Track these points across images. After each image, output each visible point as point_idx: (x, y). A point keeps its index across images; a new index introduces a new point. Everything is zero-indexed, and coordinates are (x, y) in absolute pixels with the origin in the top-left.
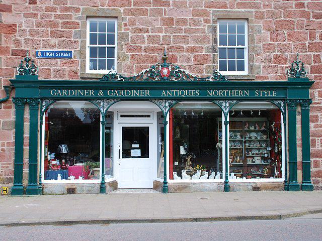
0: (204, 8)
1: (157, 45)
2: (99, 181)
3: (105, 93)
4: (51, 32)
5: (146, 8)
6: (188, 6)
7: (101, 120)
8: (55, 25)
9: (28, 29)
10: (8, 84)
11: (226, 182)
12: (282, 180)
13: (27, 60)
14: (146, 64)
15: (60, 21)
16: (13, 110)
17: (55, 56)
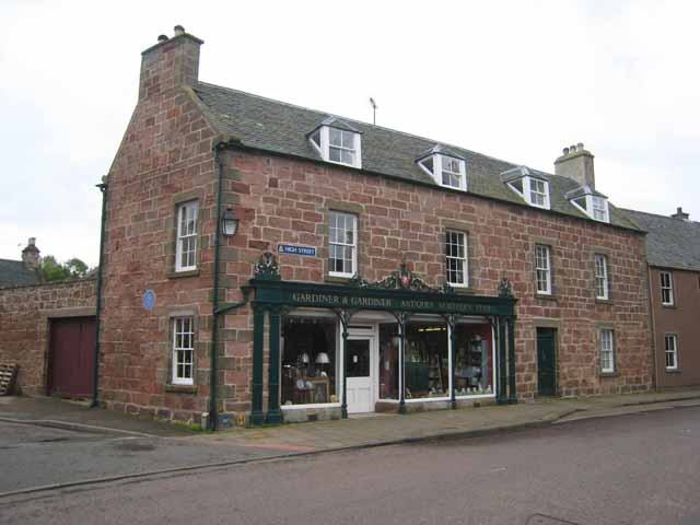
2: (398, 401)
4: (293, 222)
10: (246, 284)
11: (402, 403)
13: (268, 255)
16: (250, 317)
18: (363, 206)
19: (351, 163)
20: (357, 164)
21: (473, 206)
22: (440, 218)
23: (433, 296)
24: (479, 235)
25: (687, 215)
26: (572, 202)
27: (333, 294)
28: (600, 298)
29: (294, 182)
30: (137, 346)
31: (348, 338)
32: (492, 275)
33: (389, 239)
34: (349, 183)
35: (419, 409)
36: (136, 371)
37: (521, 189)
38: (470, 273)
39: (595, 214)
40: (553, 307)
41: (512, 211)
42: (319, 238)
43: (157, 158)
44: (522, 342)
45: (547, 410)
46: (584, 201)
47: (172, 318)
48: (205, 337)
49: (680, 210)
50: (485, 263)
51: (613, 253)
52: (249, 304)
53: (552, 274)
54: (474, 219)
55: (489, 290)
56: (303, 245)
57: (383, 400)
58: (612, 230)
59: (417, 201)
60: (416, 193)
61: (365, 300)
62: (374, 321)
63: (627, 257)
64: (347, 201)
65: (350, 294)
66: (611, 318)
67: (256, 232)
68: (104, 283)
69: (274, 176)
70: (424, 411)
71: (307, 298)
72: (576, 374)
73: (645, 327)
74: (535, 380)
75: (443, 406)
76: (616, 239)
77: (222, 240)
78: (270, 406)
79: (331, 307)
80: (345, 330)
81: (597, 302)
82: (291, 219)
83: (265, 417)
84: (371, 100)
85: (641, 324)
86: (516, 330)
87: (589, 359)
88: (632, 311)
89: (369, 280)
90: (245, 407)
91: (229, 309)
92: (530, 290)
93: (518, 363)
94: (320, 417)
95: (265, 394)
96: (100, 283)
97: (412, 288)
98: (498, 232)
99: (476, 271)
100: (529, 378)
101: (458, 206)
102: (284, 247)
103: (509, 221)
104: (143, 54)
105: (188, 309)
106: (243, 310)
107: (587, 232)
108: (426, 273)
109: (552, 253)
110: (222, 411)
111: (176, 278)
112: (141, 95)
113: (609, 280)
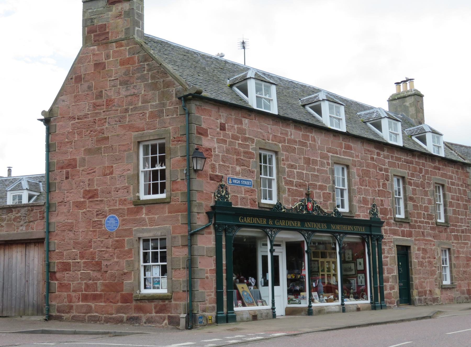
0: (326, 152)
1: (302, 181)
3: (274, 223)
4: (237, 160)
5: (295, 146)
6: (317, 148)
7: (306, 249)
8: (238, 153)
9: (221, 154)
10: (209, 210)
11: (310, 306)
13: (222, 186)
14: (297, 198)
16: (213, 236)
17: (241, 184)
18: (280, 145)
19: (270, 110)
20: (274, 110)
21: (351, 144)
22: (330, 154)
24: (355, 169)
26: (414, 138)
27: (263, 217)
28: (397, 216)
29: (236, 126)
30: (99, 264)
32: (365, 201)
33: (297, 172)
34: (271, 127)
37: (246, 93)
39: (434, 149)
40: (406, 229)
42: (253, 172)
43: (111, 101)
44: (387, 257)
46: (424, 137)
50: (360, 192)
51: (447, 182)
52: (212, 226)
53: (405, 200)
54: (351, 155)
56: (245, 178)
60: (313, 135)
63: (458, 185)
64: (270, 142)
67: (213, 167)
69: (223, 121)
70: (325, 313)
71: (248, 220)
72: (424, 284)
74: (397, 290)
75: (337, 309)
76: (450, 170)
80: (272, 247)
81: (438, 225)
82: (235, 157)
86: (383, 247)
87: (433, 273)
88: (463, 232)
89: (286, 206)
90: (212, 309)
92: (391, 215)
93: (385, 275)
98: (368, 166)
99: (354, 198)
100: (392, 288)
101: (341, 144)
102: (232, 179)
103: (375, 157)
108: (322, 200)
111: (139, 204)
112: (86, 39)
113: (445, 205)
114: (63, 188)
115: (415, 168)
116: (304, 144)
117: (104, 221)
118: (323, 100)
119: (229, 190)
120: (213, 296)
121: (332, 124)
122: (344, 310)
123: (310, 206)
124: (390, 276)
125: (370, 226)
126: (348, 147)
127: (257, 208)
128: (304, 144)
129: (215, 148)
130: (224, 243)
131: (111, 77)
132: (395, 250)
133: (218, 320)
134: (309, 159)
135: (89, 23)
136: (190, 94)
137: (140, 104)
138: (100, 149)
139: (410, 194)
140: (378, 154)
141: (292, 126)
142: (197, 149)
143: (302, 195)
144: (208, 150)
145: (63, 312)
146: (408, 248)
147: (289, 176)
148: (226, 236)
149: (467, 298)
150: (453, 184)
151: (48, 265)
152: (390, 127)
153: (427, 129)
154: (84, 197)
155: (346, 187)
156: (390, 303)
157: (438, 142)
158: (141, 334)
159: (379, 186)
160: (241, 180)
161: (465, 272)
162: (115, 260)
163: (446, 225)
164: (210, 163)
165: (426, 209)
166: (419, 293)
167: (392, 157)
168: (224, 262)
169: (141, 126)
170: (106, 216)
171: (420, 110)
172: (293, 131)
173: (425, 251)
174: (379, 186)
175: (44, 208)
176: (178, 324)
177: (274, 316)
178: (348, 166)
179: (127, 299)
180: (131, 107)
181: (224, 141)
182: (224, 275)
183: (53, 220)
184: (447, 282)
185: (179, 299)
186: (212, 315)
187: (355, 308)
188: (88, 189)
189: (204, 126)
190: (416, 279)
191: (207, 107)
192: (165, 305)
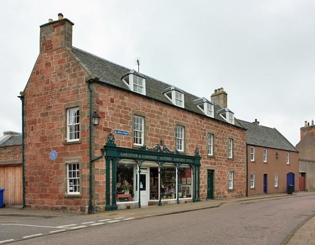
2: (159, 201)
4: (120, 120)
7: (159, 171)
8: (121, 116)
10: (103, 148)
11: (160, 201)
12: (192, 198)
13: (111, 135)
15: (124, 114)
18: (147, 113)
20: (144, 93)
22: (175, 120)
23: (171, 155)
25: (259, 122)
28: (209, 154)
30: (47, 178)
31: (141, 173)
35: (166, 203)
36: (47, 189)
38: (185, 146)
41: (200, 118)
42: (130, 127)
43: (54, 85)
44: (202, 176)
45: (211, 203)
47: (67, 164)
48: (86, 172)
49: (256, 120)
50: (190, 141)
52: (104, 157)
53: (214, 146)
54: (186, 121)
55: (191, 153)
57: (151, 201)
58: (235, 128)
59: (166, 112)
60: (165, 108)
61: (177, 159)
62: (147, 166)
63: (240, 140)
64: (141, 111)
65: (141, 153)
66: (233, 166)
68: (25, 147)
69: (112, 97)
71: (126, 155)
72: (220, 189)
73: (244, 170)
74: (206, 192)
75: (175, 202)
76: (236, 132)
77: (93, 127)
78: (113, 203)
79: (134, 159)
81: (228, 159)
82: (119, 118)
83: (111, 207)
84: (138, 61)
85: (243, 168)
86: (200, 170)
90: (103, 203)
91: (97, 159)
93: (201, 184)
94: (131, 207)
95: (111, 197)
96: (23, 147)
97: (165, 152)
98: (195, 128)
100: (204, 191)
102: (117, 131)
103: (199, 123)
104: (41, 27)
105: (75, 159)
106: (102, 160)
107: (226, 128)
108: (169, 145)
109: (213, 137)
110: (95, 205)
111: (67, 144)
113: (233, 150)
114: (30, 136)
115: (219, 130)
116: (161, 114)
117: (50, 154)
118: (173, 90)
119: (115, 138)
120: (104, 196)
121: (177, 103)
122: (178, 203)
123: (162, 147)
124: (203, 185)
125: (194, 159)
126: (185, 117)
127: (132, 148)
128: (161, 114)
129: (107, 112)
130: (111, 167)
131: (53, 71)
132: (206, 171)
133: (107, 209)
134: (163, 122)
135: (43, 40)
136: (92, 79)
137: (67, 86)
138: (47, 113)
139: (216, 144)
140: (201, 122)
141: (154, 103)
142: (95, 112)
143: (158, 142)
144: (103, 113)
145: (31, 203)
146: (213, 171)
147: (151, 131)
148: (112, 163)
149: (239, 195)
150: (237, 139)
151: (24, 178)
152: (208, 108)
153: (227, 110)
154: (40, 141)
155: (183, 138)
156: (203, 198)
157: (232, 117)
158: (34, 218)
159: (200, 138)
160: (122, 132)
161: (240, 183)
162: (55, 176)
163: (233, 159)
164: (104, 121)
165: (224, 151)
166: (218, 194)
167: (208, 123)
168: (111, 177)
169: (67, 99)
170: (50, 151)
171: (225, 101)
172: (154, 106)
173: (221, 172)
174: (200, 138)
175: (21, 147)
176: (84, 211)
177: (140, 206)
178: (184, 127)
179: (60, 197)
180: (63, 88)
181: (113, 109)
182: (111, 185)
183: (26, 154)
184: (231, 188)
185: (86, 198)
186: (103, 206)
187: (126, 207)
188: (42, 136)
189: (100, 99)
190: (216, 187)
191: (103, 88)
192: (78, 201)
